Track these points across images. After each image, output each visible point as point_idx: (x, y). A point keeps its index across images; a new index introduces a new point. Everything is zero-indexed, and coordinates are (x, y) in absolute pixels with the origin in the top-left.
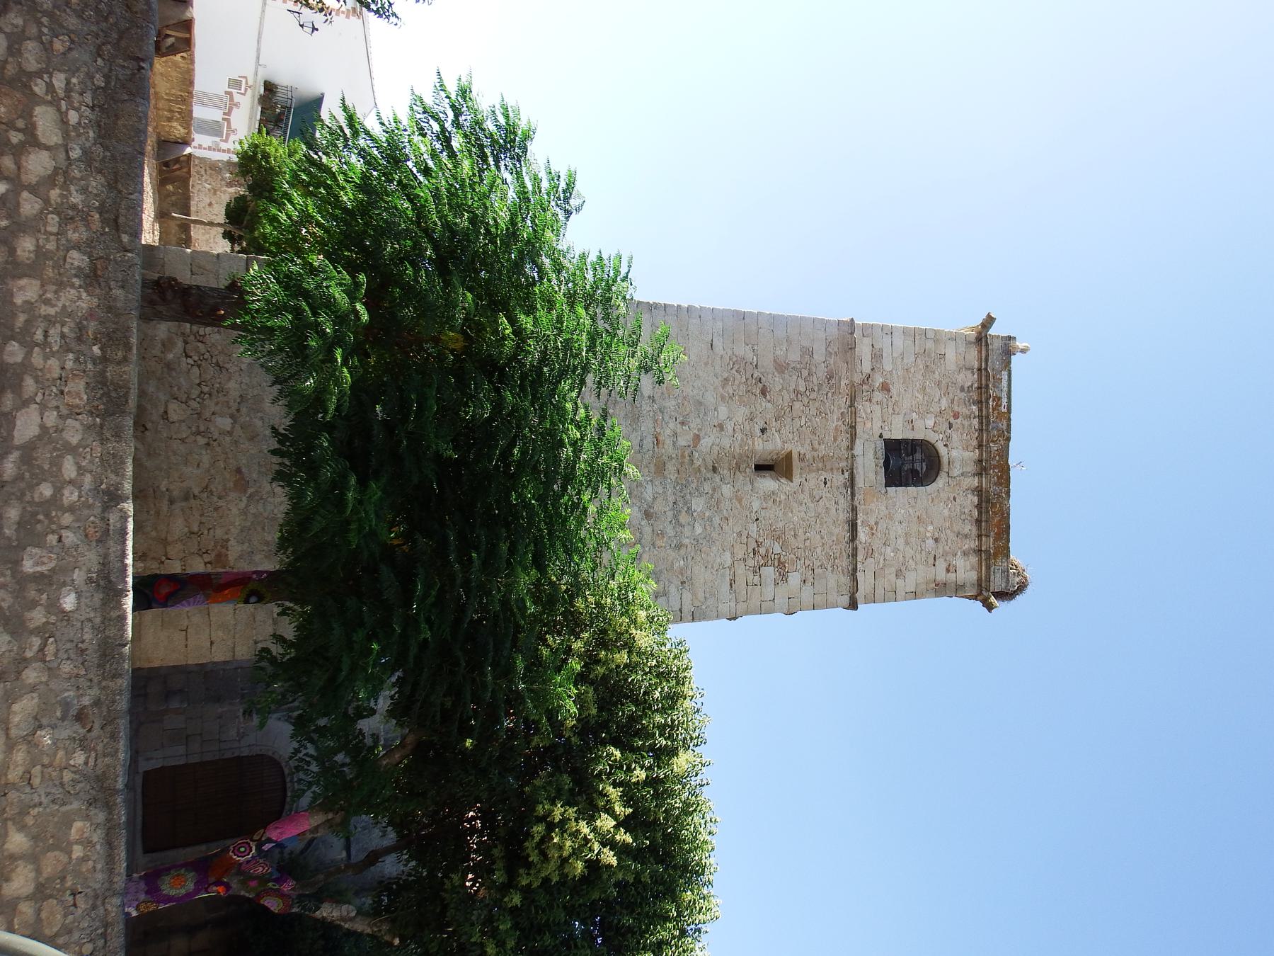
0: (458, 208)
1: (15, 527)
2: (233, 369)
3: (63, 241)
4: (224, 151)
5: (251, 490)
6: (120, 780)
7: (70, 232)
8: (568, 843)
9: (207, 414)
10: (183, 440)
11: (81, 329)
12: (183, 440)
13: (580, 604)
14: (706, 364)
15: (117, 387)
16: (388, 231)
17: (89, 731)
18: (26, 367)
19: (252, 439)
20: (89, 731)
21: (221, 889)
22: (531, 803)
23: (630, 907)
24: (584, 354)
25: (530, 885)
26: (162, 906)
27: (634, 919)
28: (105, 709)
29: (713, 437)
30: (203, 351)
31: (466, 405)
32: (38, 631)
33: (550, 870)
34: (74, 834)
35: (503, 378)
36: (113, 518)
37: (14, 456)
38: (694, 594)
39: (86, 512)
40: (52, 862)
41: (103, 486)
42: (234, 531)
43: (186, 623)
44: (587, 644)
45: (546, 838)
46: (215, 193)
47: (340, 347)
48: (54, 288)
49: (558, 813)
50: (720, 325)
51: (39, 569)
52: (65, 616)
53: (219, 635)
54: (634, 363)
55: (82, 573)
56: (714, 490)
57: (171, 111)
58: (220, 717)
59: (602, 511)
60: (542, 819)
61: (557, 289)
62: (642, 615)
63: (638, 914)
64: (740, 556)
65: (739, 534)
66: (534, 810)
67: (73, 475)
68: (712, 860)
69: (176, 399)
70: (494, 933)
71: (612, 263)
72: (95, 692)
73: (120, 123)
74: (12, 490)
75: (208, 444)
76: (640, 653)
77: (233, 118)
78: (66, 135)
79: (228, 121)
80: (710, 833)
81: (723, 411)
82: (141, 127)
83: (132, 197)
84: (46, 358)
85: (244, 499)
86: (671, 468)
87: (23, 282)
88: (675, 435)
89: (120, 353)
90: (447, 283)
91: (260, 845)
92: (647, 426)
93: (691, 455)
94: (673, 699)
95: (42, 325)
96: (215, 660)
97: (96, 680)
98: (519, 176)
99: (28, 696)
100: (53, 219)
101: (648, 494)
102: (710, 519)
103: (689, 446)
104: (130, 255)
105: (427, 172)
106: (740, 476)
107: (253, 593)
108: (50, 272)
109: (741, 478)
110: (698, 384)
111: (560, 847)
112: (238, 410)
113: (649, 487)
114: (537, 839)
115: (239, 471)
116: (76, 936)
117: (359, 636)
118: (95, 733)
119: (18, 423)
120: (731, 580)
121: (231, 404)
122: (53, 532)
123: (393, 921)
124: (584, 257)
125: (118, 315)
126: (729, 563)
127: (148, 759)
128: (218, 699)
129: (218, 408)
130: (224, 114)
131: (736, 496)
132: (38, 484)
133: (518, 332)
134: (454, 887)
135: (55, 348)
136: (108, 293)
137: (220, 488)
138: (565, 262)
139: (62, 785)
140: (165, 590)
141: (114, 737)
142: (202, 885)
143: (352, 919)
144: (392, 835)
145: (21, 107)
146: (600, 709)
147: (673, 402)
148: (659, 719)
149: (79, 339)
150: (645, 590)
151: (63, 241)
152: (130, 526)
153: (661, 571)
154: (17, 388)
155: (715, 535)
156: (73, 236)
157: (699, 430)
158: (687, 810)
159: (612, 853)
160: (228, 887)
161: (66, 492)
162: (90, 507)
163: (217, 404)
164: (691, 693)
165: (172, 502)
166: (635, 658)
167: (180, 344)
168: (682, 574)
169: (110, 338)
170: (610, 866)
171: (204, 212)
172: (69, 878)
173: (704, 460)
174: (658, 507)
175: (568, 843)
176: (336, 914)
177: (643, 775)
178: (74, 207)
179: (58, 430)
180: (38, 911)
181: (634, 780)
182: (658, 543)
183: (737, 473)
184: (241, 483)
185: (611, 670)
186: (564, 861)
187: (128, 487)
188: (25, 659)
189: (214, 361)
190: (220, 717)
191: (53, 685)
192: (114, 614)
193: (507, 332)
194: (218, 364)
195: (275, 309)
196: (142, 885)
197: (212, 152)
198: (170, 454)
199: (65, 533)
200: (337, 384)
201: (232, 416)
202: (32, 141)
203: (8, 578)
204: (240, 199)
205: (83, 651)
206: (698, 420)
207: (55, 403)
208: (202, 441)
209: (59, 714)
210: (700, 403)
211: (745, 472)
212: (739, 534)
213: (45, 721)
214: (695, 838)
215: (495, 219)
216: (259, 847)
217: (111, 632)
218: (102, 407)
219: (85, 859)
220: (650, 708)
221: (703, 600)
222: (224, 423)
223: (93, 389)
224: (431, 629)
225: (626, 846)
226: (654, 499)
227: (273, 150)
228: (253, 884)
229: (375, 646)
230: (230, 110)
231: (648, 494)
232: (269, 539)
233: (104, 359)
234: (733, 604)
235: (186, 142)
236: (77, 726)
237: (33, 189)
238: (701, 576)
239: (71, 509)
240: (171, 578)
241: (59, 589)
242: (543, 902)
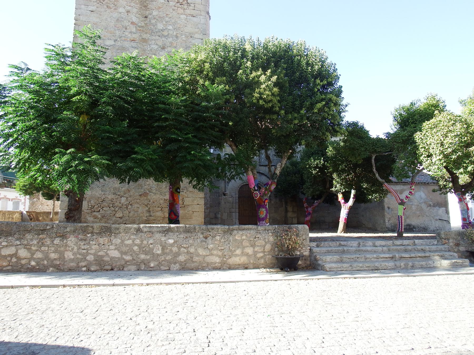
0: (25, 113)
1: (147, 256)
2: (104, 197)
3: (51, 245)
4: (25, 201)
5: (148, 192)
6: (226, 227)
7: (47, 243)
8: (267, 92)
9: (120, 205)
10: (129, 212)
11: (81, 240)
12: (129, 212)
13: (187, 79)
14: (100, 15)
15: (102, 229)
16: (37, 140)
17: (210, 235)
18: (94, 255)
19: (129, 191)
20: (210, 235)
21: (266, 201)
22: (253, 105)
23: (294, 73)
24: (86, 69)
25: (279, 107)
26: (268, 217)
27: (298, 72)
28: (205, 231)
29: (132, 16)
30: (97, 206)
31: (108, 115)
32: (179, 249)
33: (275, 100)
34: (239, 238)
35: (97, 101)
36: (145, 230)
37: (124, 257)
38: (196, 33)
39: (143, 237)
40: (246, 243)
41: (135, 233)
42: (161, 197)
44: (201, 78)
45: (264, 100)
46: (43, 204)
47: (84, 159)
48: (67, 247)
49: (256, 95)
50: (83, 6)
51: (160, 249)
52: (175, 242)
53: (196, 202)
54: (91, 47)
55: (163, 238)
56: (155, 19)
57: (9, 218)
58: (225, 203)
59: (153, 67)
60: (258, 101)
61: (60, 77)
62: (193, 56)
63: (297, 70)
64: (183, 11)
65: (173, 10)
66: (255, 103)
67: (131, 241)
68: (285, 40)
69: (115, 214)
70: (291, 120)
71: (47, 52)
72: (199, 234)
73: (5, 229)
74: (135, 257)
75: (131, 205)
76: (207, 59)
77: (11, 198)
78: (12, 245)
79: (12, 199)
80: (276, 40)
81: (121, 10)
82: (6, 223)
83: (33, 226)
84: (92, 249)
85: (150, 194)
86: (145, 36)
87: (66, 256)
88: (131, 32)
89: (90, 229)
90: (60, 120)
91: (255, 190)
92: (127, 44)
93: (140, 27)
94: (225, 47)
95: (81, 250)
96: (203, 203)
97: (196, 234)
98: (12, 88)
99: (198, 251)
100: (43, 248)
101: (155, 47)
102: (167, 22)
103: (136, 27)
104: (54, 226)
105: (14, 125)
106: (149, 6)
107: (176, 190)
108: (62, 249)
109: (150, 6)
110: (109, 19)
111: (268, 95)
112: (119, 195)
113: (152, 46)
114: (264, 103)
115: (140, 195)
116: (266, 237)
117: (189, 157)
118: (211, 234)
119: (113, 256)
120: (192, 16)
121: (116, 197)
122: (149, 246)
123: (284, 152)
124: (47, 64)
125: (76, 229)
126: (185, 16)
128: (219, 203)
129: (118, 202)
130: (9, 200)
131: (158, 9)
132: (134, 250)
133: (78, 93)
134: (276, 132)
135: (89, 247)
136: (69, 232)
137: (147, 201)
138: (49, 72)
139: (225, 242)
140: (173, 216)
141: (213, 229)
142: (264, 206)
143: (282, 164)
144: (263, 151)
145: (3, 259)
146: (225, 76)
147: (117, 32)
148: (231, 54)
149: (85, 240)
150: (182, 53)
151: (51, 245)
152: (148, 225)
153: (186, 45)
154: (102, 256)
155: (173, 21)
156: (49, 242)
157: (129, 21)
158: (266, 48)
159: (273, 77)
160: (266, 199)
161: (136, 243)
162: (141, 236)
163: (117, 202)
164: (225, 40)
165: (151, 216)
166: (208, 60)
167: (95, 213)
168: (188, 37)
169: (85, 231)
170: (277, 79)
171: (51, 208)
172: (251, 239)
173: (142, 21)
174: (160, 43)
175: (267, 92)
176: (279, 169)
177: (249, 63)
178: (38, 243)
179: (116, 245)
180: (258, 246)
181: (250, 66)
182: (175, 45)
183: (148, 7)
184: (145, 194)
185: (211, 70)
186: (273, 94)
187: (135, 226)
188: (187, 252)
189: (101, 203)
190: (225, 203)
191: (196, 245)
192: (176, 229)
193: (78, 98)
194: (102, 202)
195: (70, 180)
196: (261, 222)
197: (26, 205)
198: (134, 216)
199: (149, 243)
200: (98, 160)
201: (121, 197)
202: (15, 255)
203: (162, 257)
204: (43, 195)
205: (186, 237)
206: (125, 21)
207: (107, 246)
208: (130, 207)
209: (204, 243)
210: (118, 20)
211: (148, 4)
212: (173, 10)
213: (206, 247)
214: (277, 46)
215: (30, 99)
216: (256, 190)
217: (181, 230)
218: (108, 233)
219: (246, 236)
220: (227, 57)
221: (198, 29)
222: (123, 200)
223: (102, 236)
224: (189, 134)
225: (271, 72)
226: (157, 45)
227: (21, 183)
228: (266, 192)
229: (192, 152)
230: (7, 198)
231: (155, 47)
232: (164, 186)
233: (92, 233)
234: (201, 17)
235: (22, 213)
236: (208, 238)
237: (33, 254)
238: (189, 29)
239: (142, 241)
240: (170, 215)
241: (167, 244)
242: (286, 103)
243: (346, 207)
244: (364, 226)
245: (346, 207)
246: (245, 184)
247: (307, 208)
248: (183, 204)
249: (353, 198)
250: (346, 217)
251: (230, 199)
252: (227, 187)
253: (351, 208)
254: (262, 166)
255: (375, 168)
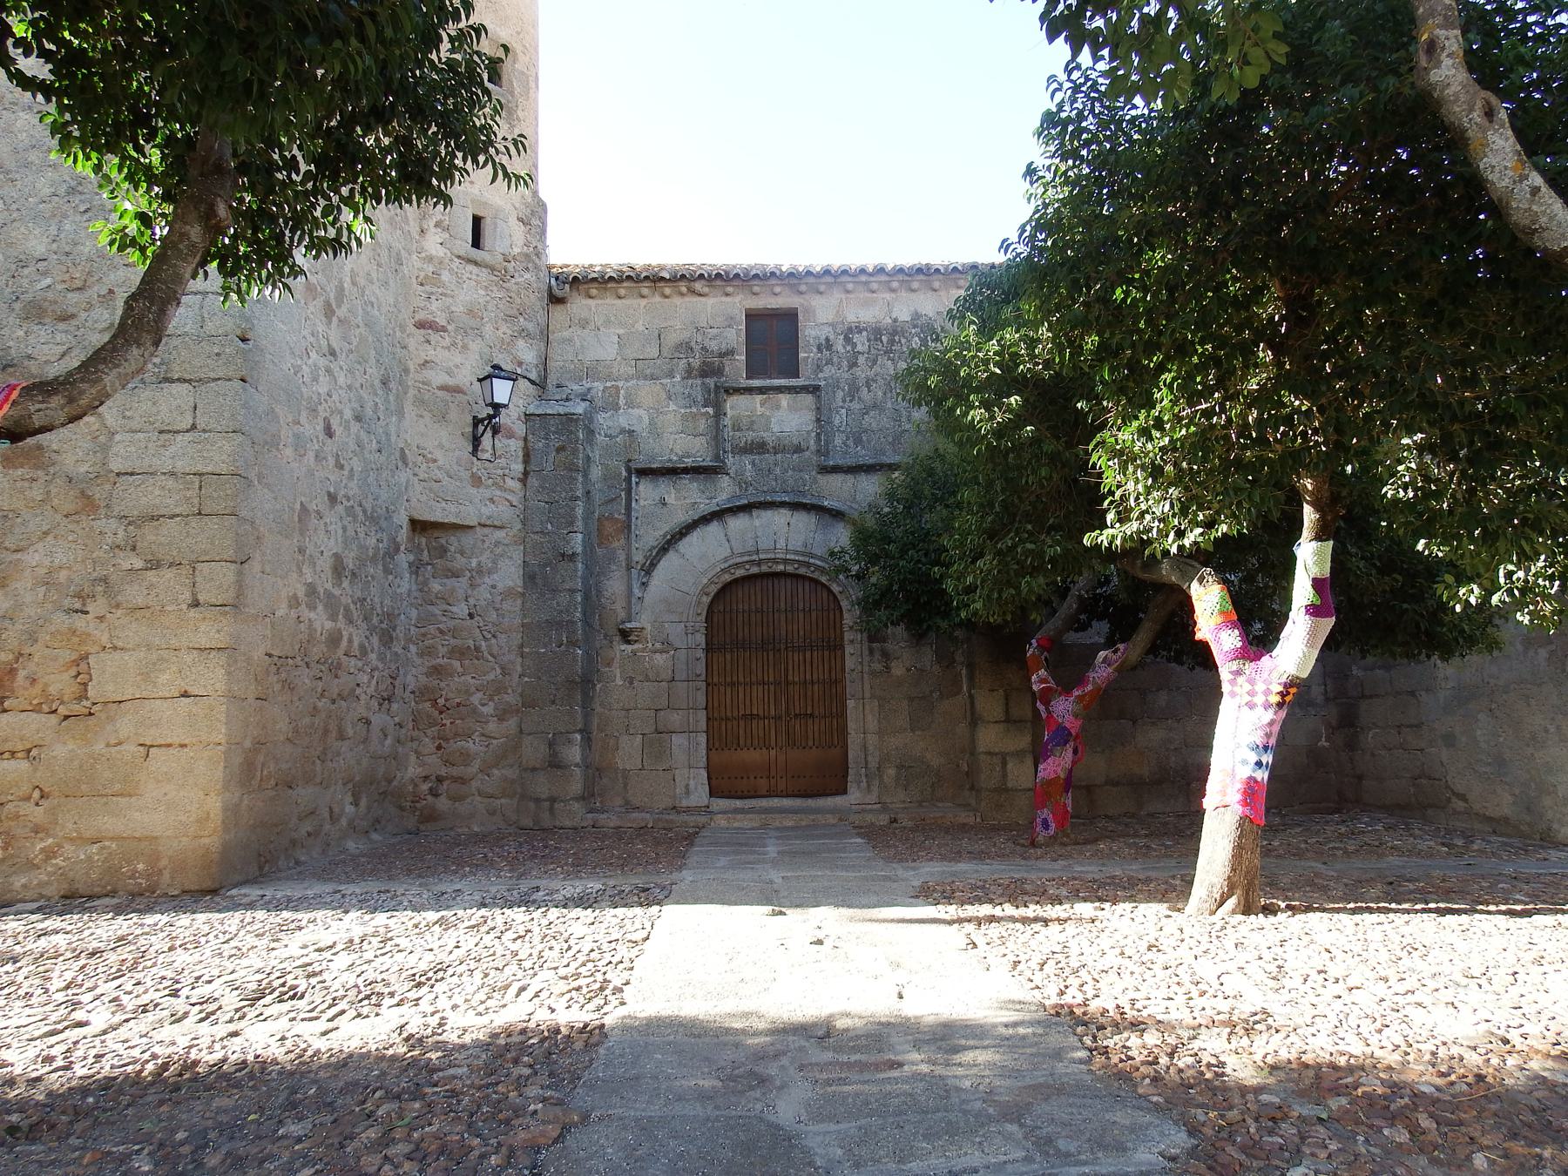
43: (130, 748)
53: (167, 681)
127: (688, 792)
243: (1260, 687)
244: (1459, 805)
245: (1260, 687)
246: (740, 573)
247: (1046, 697)
248: (82, 696)
249: (1314, 611)
250: (1262, 775)
251: (660, 659)
252: (637, 592)
253: (1296, 696)
254: (835, 469)
255: (1452, 41)
